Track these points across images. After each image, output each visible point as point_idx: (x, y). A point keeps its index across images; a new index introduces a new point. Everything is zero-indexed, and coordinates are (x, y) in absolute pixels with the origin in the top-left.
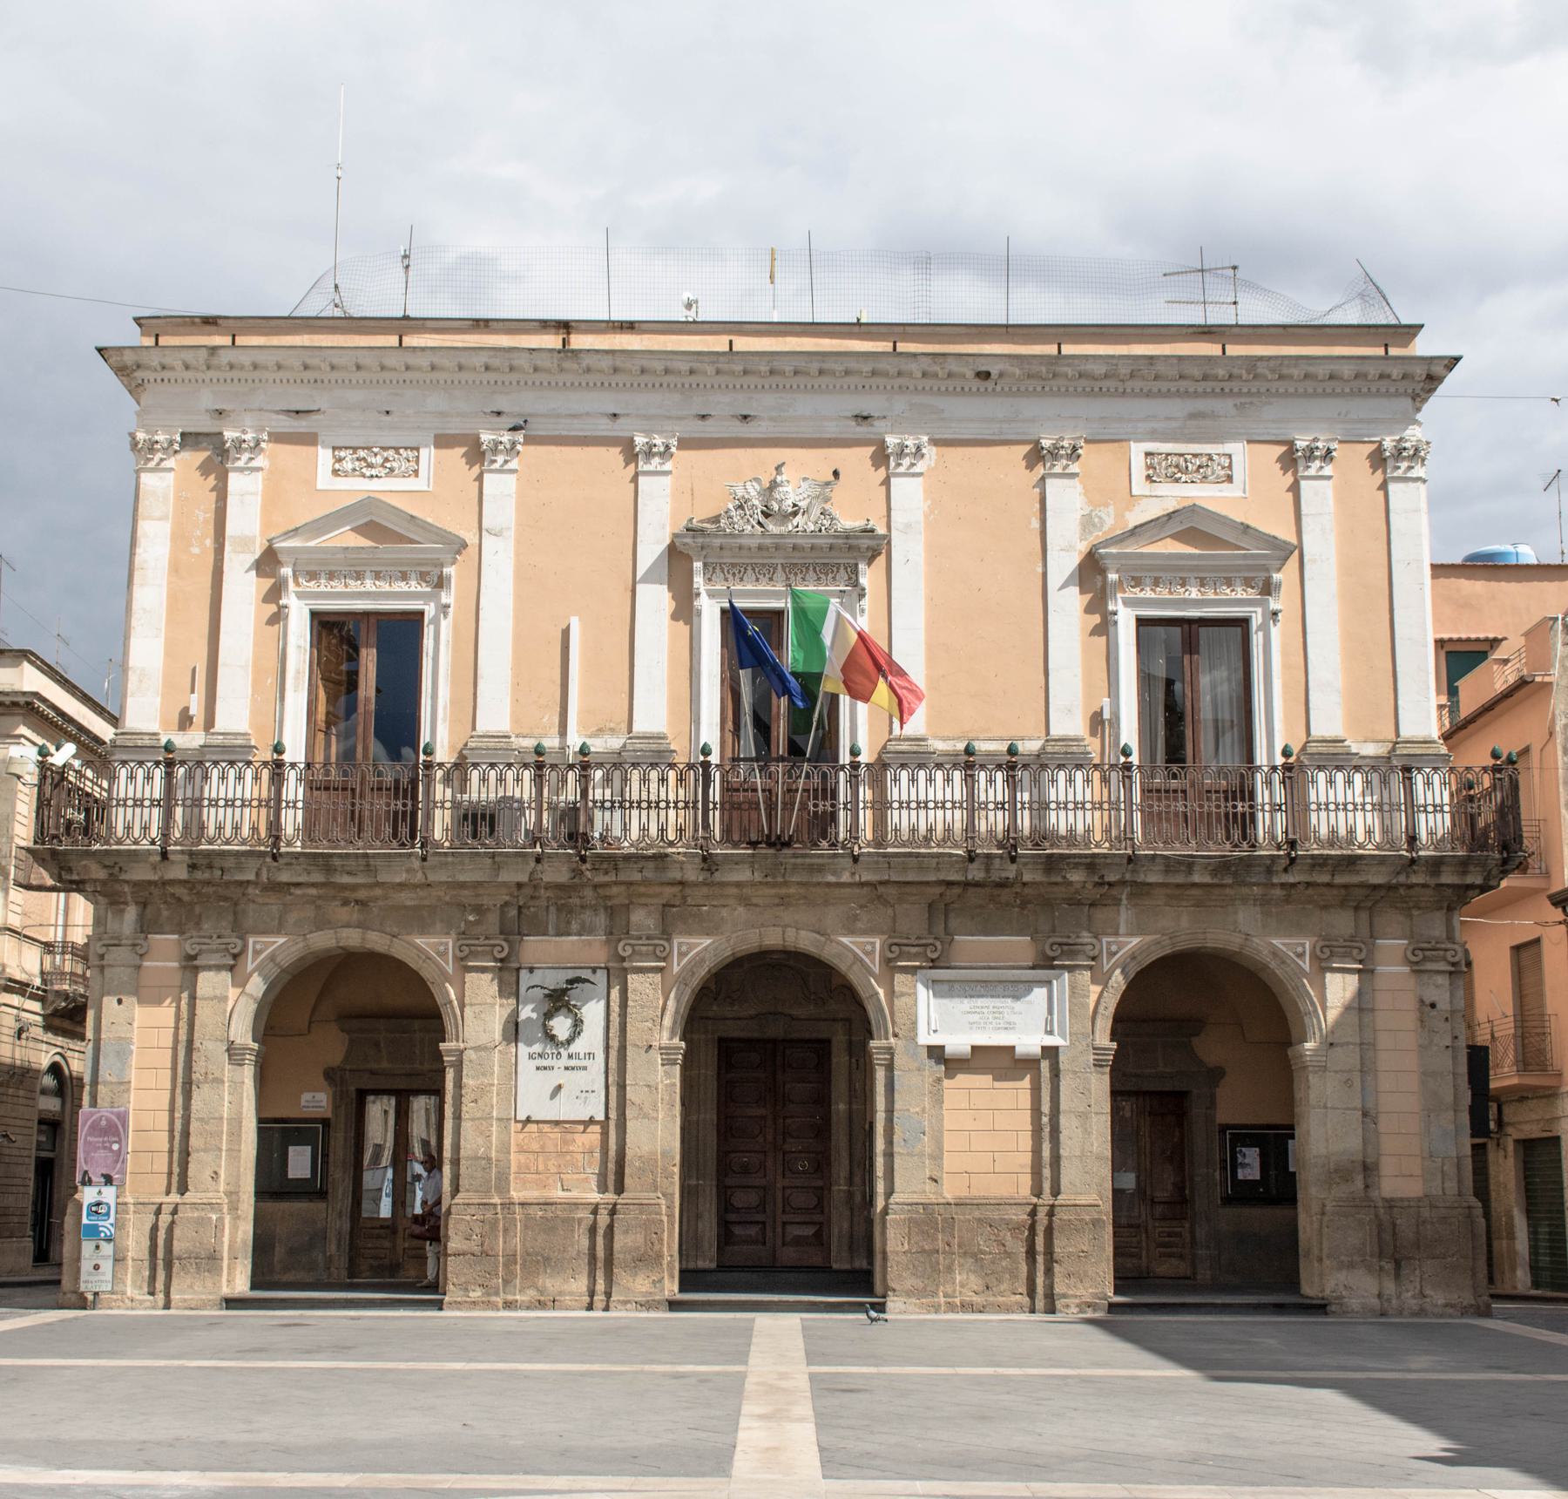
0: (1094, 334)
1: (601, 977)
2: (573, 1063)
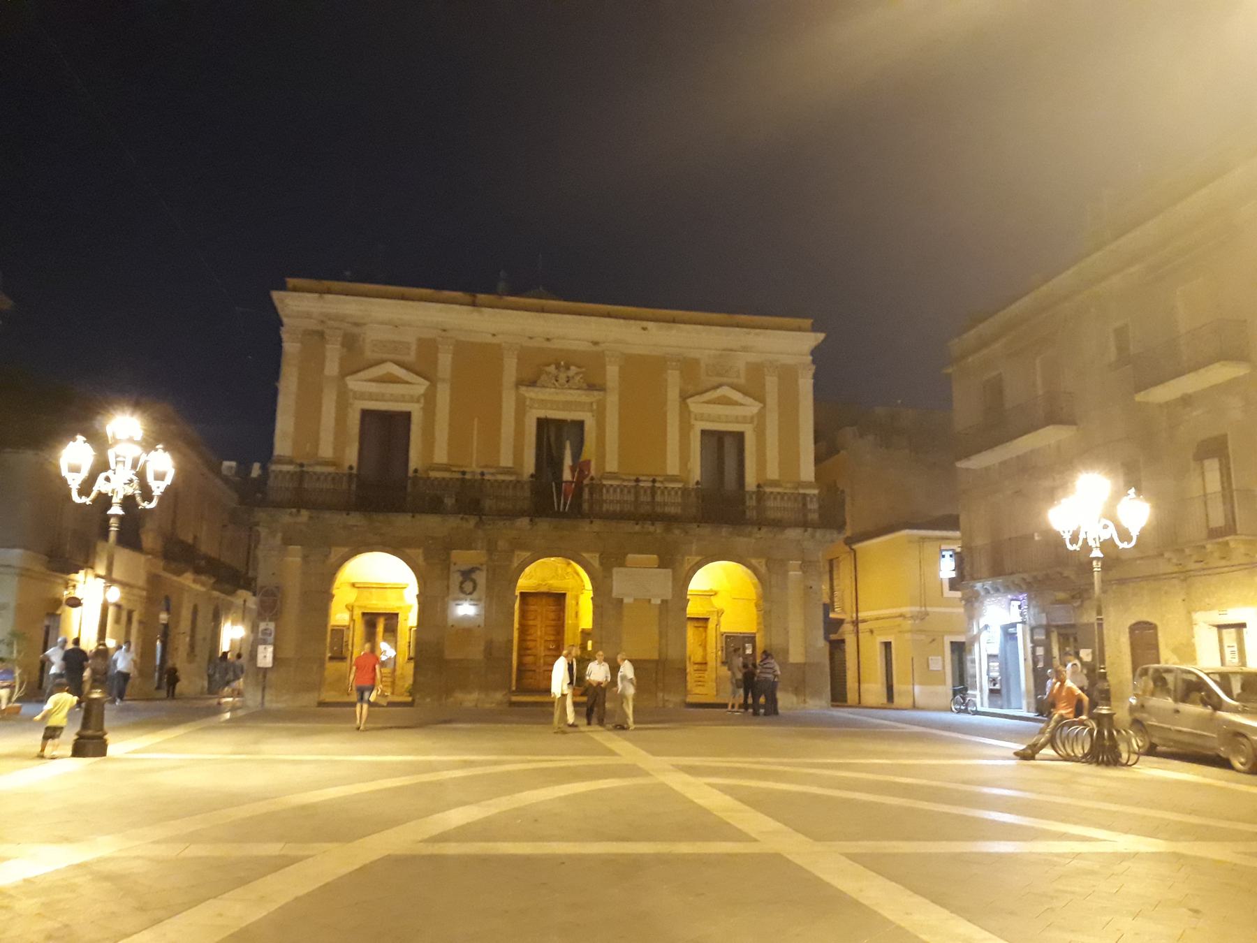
1: (484, 567)
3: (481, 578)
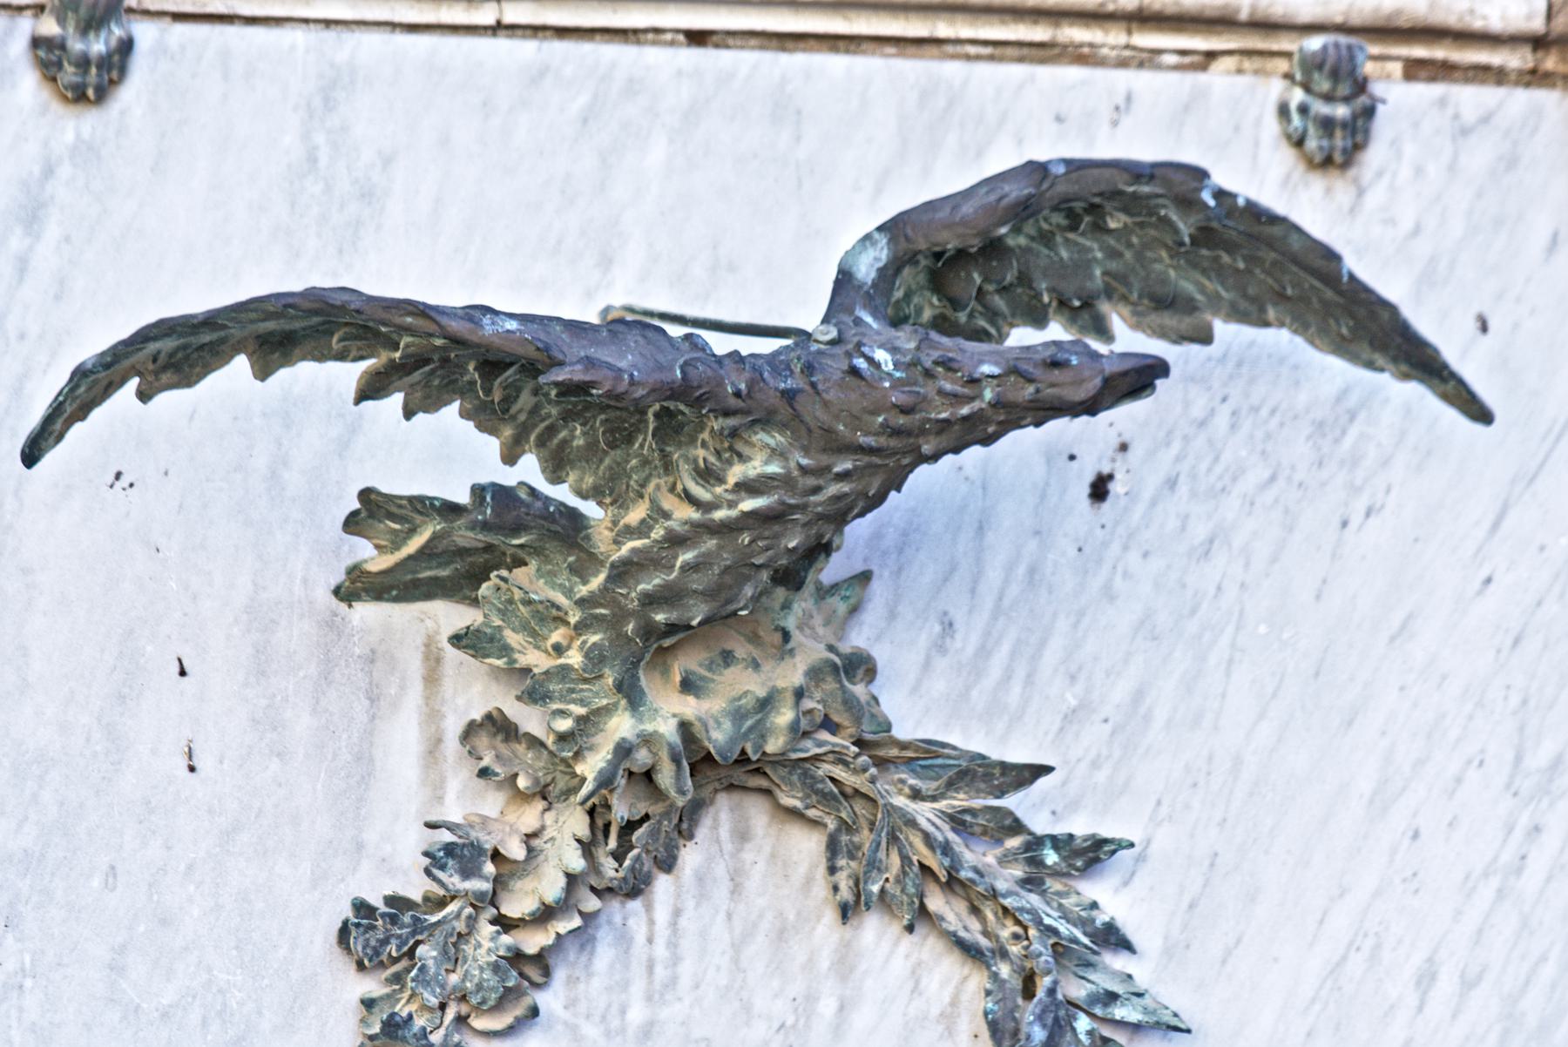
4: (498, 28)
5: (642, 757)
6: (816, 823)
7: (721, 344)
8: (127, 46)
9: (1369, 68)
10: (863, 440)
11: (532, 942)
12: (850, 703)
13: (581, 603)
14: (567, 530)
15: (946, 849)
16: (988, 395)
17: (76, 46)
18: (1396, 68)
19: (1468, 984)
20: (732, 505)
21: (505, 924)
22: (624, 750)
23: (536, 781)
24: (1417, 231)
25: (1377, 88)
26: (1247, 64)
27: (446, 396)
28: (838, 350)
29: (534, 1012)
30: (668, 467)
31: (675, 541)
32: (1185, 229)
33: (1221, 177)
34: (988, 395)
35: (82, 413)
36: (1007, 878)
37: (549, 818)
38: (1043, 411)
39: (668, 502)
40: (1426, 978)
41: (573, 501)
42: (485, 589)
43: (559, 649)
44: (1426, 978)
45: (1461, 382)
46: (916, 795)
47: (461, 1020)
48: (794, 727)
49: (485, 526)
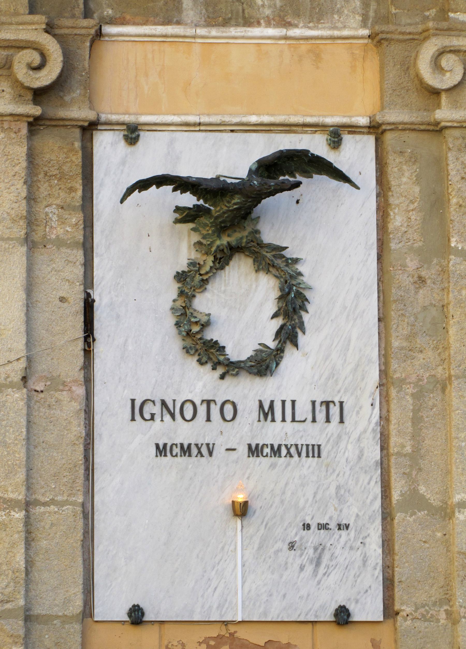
0: (88, 532)
1: (356, 156)
2: (275, 432)
3: (330, 234)
4: (200, 131)
5: (221, 247)
6: (251, 257)
7: (229, 181)
8: (138, 136)
9: (341, 132)
10: (253, 196)
11: (205, 277)
12: (256, 238)
13: (211, 223)
14: (208, 211)
15: (272, 260)
16: (272, 188)
17: (130, 136)
18: (346, 132)
19: (358, 280)
20: (232, 207)
21: (201, 275)
22: (218, 247)
23: (205, 252)
24: (349, 159)
25: (343, 136)
26: (322, 132)
27: (322, 173)
28: (248, 182)
29: (206, 289)
30: (223, 201)
31: (224, 213)
32: (306, 160)
33: (312, 151)
34: (272, 188)
35: (129, 195)
36: (282, 265)
37: (208, 257)
38: (282, 190)
39: (223, 207)
40: (352, 279)
41: (209, 207)
42: (196, 221)
43: (208, 231)
44: (352, 279)
45: (354, 183)
46: (267, 252)
47: (194, 290)
48: (246, 242)
49: (195, 211)
